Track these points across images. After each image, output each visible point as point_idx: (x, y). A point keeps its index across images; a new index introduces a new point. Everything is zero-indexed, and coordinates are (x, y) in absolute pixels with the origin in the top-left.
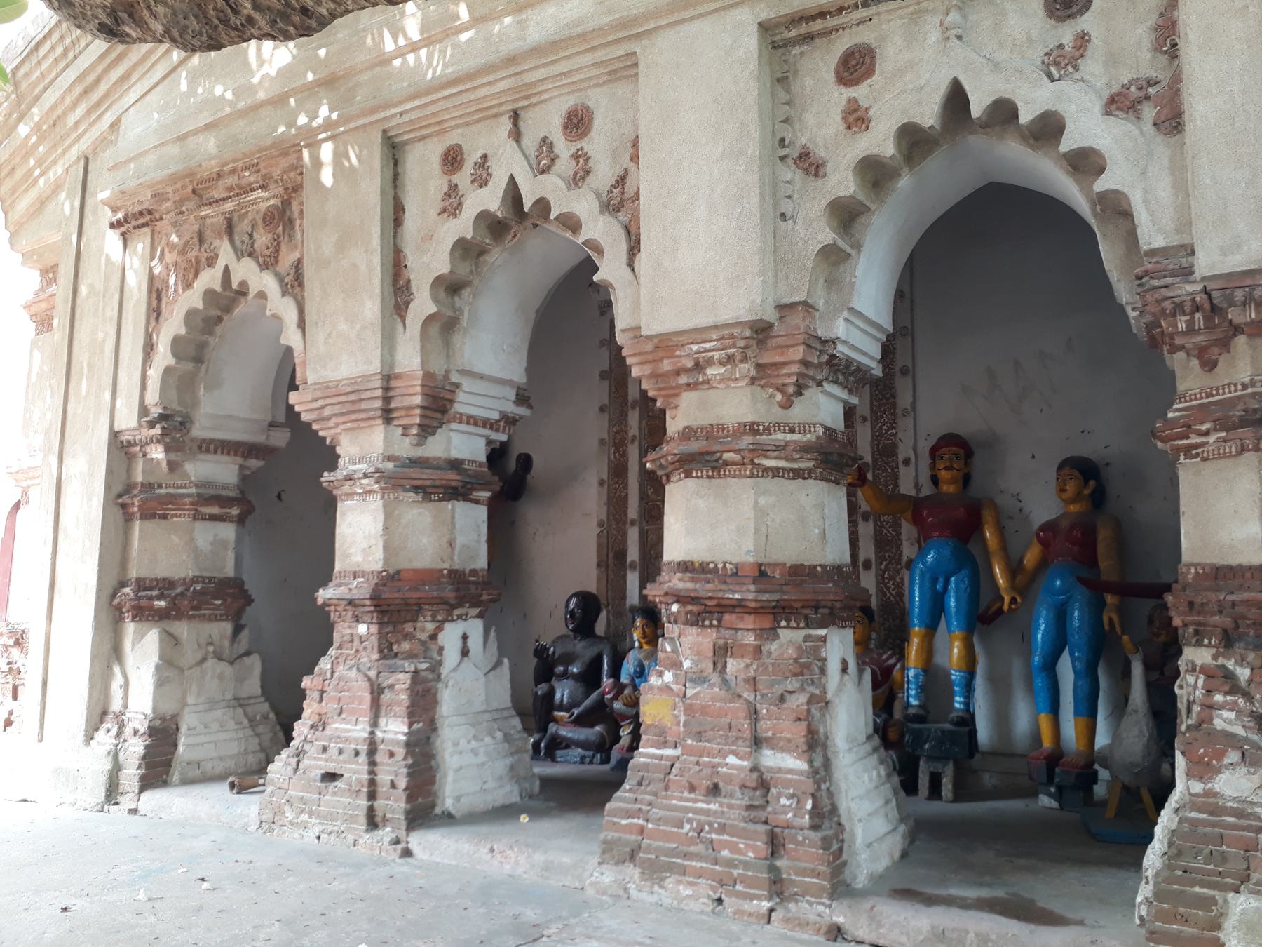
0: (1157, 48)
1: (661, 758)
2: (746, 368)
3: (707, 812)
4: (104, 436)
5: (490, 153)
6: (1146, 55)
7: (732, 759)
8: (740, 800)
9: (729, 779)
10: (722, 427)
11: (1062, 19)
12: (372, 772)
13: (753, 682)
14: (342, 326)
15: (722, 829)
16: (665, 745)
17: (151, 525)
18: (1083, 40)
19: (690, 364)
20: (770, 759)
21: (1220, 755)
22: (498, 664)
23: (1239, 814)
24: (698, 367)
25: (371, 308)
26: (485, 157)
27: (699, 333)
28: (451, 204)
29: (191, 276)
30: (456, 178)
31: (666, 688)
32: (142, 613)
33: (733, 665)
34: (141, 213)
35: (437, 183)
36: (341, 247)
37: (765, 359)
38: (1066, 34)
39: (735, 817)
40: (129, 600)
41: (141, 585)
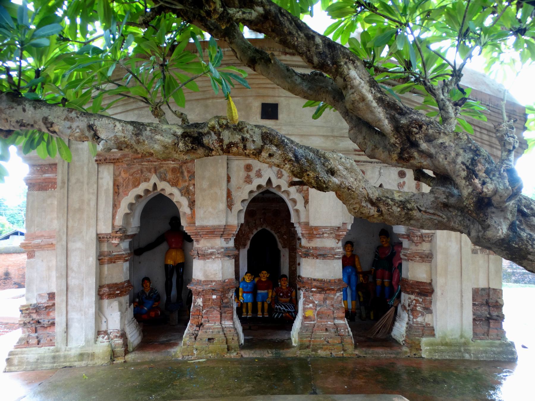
0: (416, 188)
1: (311, 324)
2: (334, 235)
3: (327, 335)
4: (94, 235)
5: (261, 168)
6: (414, 189)
7: (329, 323)
8: (333, 331)
9: (330, 327)
10: (326, 248)
11: (401, 178)
12: (225, 337)
13: (332, 305)
14: (210, 209)
15: (331, 338)
16: (311, 321)
17: (110, 265)
18: (404, 183)
19: (321, 233)
20: (337, 322)
21: (418, 314)
22: (130, 305)
23: (421, 324)
24: (323, 234)
25: (223, 205)
26: (260, 170)
27: (325, 227)
28: (248, 180)
29: (137, 184)
30: (250, 173)
31: (310, 308)
32: (112, 296)
33: (328, 302)
34: (114, 159)
35: (243, 174)
36: (211, 186)
37: (338, 233)
38: (402, 181)
39: (333, 335)
40: (105, 292)
41: (110, 286)
